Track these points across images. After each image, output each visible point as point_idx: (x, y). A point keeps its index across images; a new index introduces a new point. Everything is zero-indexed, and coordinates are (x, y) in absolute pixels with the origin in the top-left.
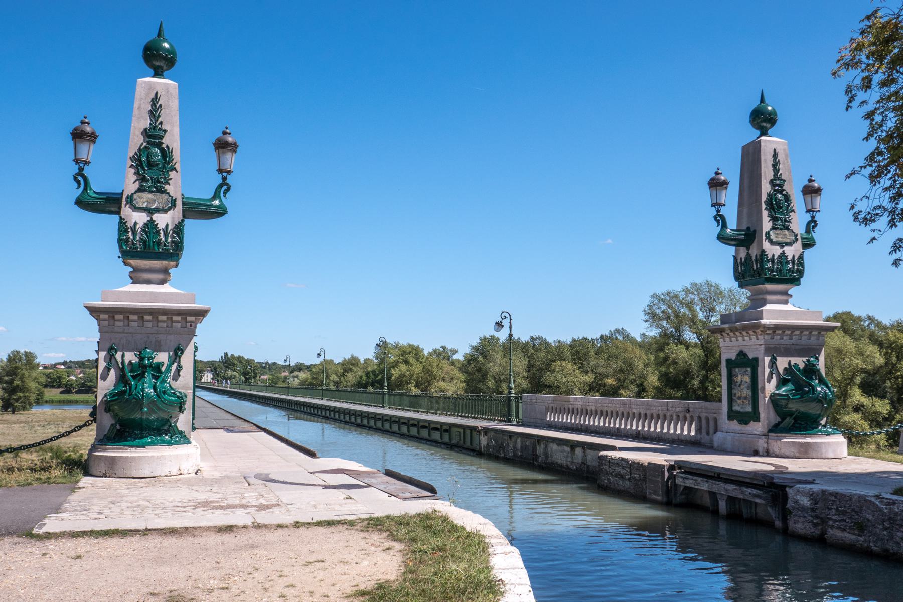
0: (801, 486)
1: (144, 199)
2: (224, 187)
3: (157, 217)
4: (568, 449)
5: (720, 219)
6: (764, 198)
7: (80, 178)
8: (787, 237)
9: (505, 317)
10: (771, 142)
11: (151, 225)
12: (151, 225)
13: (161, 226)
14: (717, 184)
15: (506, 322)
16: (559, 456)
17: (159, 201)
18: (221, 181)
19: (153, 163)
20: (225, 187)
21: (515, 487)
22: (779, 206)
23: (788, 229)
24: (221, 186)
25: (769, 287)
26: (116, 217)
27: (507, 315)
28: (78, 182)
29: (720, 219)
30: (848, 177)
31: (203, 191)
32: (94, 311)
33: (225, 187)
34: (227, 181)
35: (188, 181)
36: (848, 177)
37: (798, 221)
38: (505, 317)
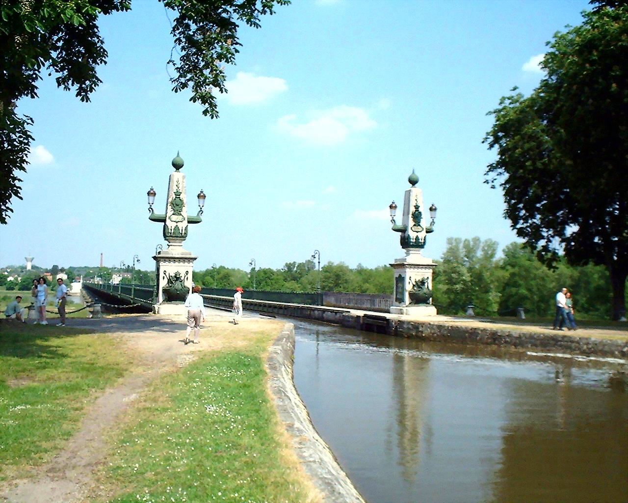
0: (540, 354)
1: (174, 218)
2: (201, 211)
3: (179, 224)
4: (334, 314)
5: (393, 221)
6: (411, 213)
7: (150, 209)
8: (419, 229)
9: (317, 253)
10: (416, 190)
11: (177, 227)
12: (177, 227)
14: (151, 193)
15: (317, 256)
16: (328, 315)
17: (179, 218)
18: (200, 210)
19: (177, 205)
20: (201, 212)
21: (321, 337)
22: (417, 217)
23: (419, 225)
25: (411, 249)
27: (317, 252)
28: (150, 211)
29: (393, 221)
31: (194, 214)
32: (152, 257)
33: (201, 212)
34: (202, 209)
35: (190, 210)
37: (425, 222)
38: (317, 253)
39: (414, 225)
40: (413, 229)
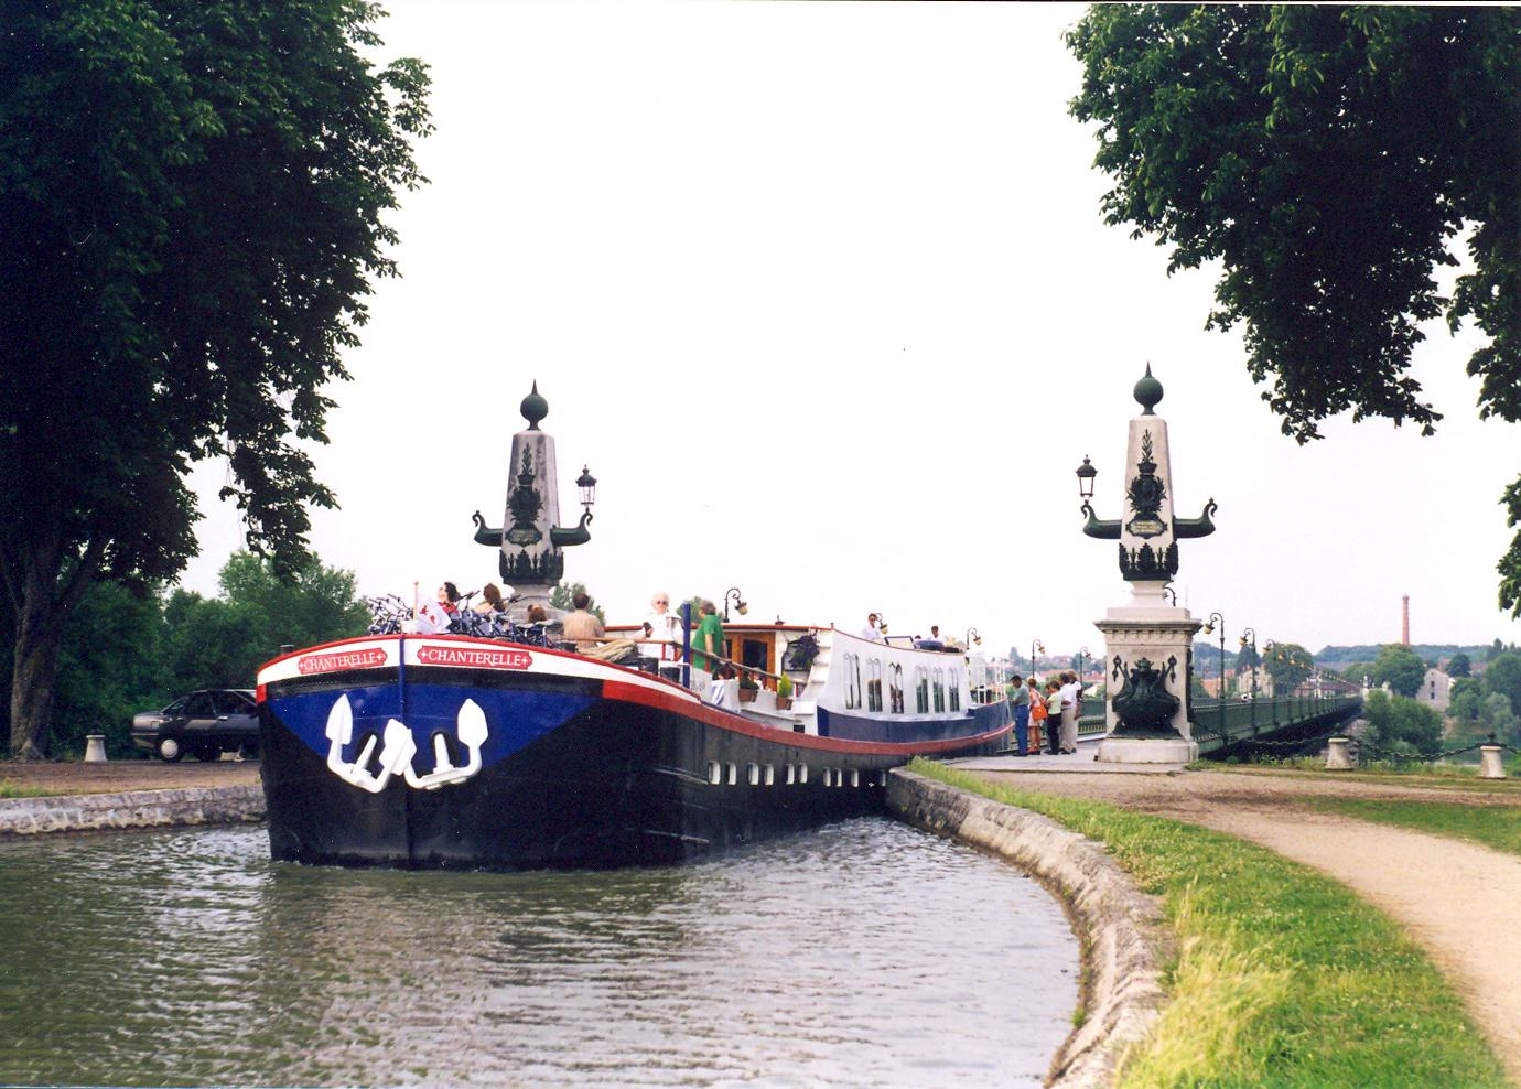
13: (531, 556)
14: (1087, 471)
24: (584, 517)
26: (493, 552)
30: (1406, 599)
36: (1406, 599)
39: (1138, 518)
40: (1133, 527)
